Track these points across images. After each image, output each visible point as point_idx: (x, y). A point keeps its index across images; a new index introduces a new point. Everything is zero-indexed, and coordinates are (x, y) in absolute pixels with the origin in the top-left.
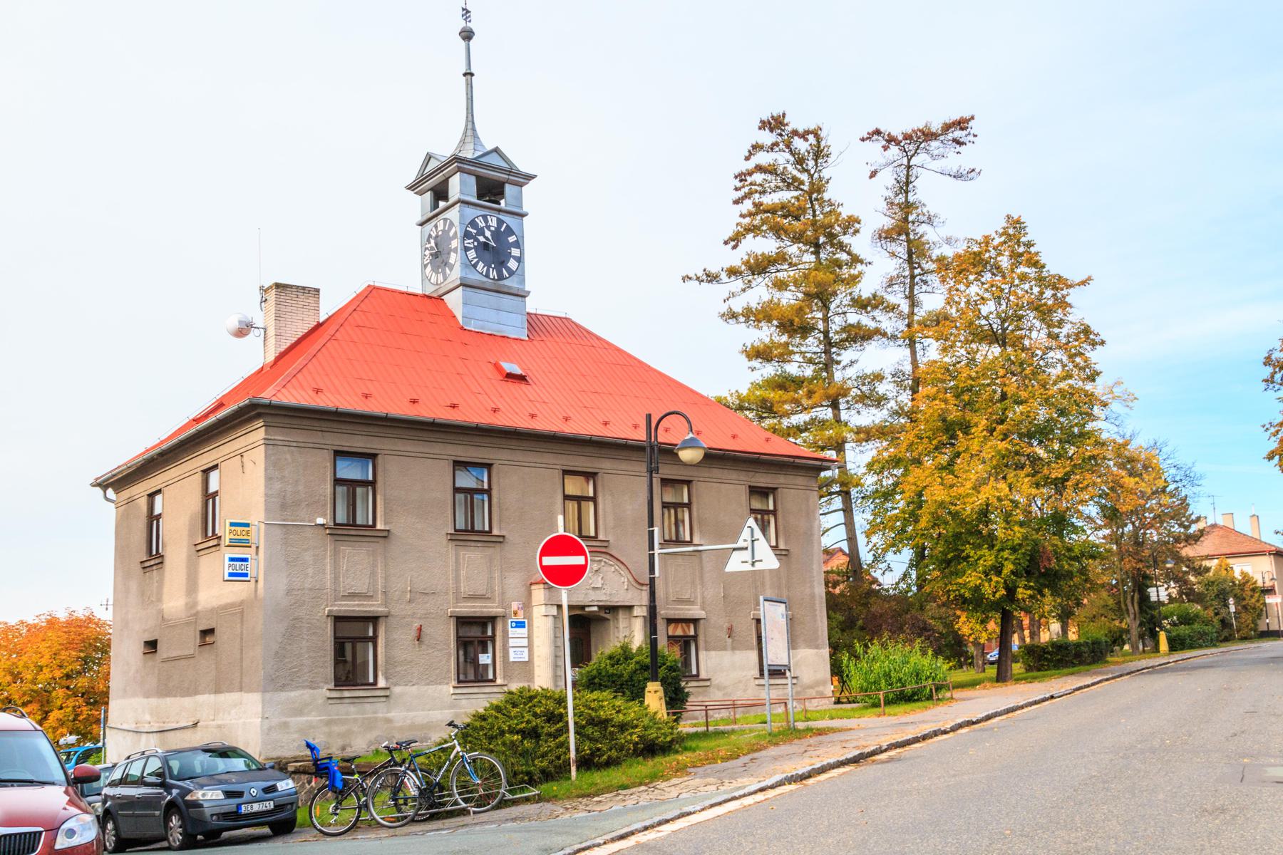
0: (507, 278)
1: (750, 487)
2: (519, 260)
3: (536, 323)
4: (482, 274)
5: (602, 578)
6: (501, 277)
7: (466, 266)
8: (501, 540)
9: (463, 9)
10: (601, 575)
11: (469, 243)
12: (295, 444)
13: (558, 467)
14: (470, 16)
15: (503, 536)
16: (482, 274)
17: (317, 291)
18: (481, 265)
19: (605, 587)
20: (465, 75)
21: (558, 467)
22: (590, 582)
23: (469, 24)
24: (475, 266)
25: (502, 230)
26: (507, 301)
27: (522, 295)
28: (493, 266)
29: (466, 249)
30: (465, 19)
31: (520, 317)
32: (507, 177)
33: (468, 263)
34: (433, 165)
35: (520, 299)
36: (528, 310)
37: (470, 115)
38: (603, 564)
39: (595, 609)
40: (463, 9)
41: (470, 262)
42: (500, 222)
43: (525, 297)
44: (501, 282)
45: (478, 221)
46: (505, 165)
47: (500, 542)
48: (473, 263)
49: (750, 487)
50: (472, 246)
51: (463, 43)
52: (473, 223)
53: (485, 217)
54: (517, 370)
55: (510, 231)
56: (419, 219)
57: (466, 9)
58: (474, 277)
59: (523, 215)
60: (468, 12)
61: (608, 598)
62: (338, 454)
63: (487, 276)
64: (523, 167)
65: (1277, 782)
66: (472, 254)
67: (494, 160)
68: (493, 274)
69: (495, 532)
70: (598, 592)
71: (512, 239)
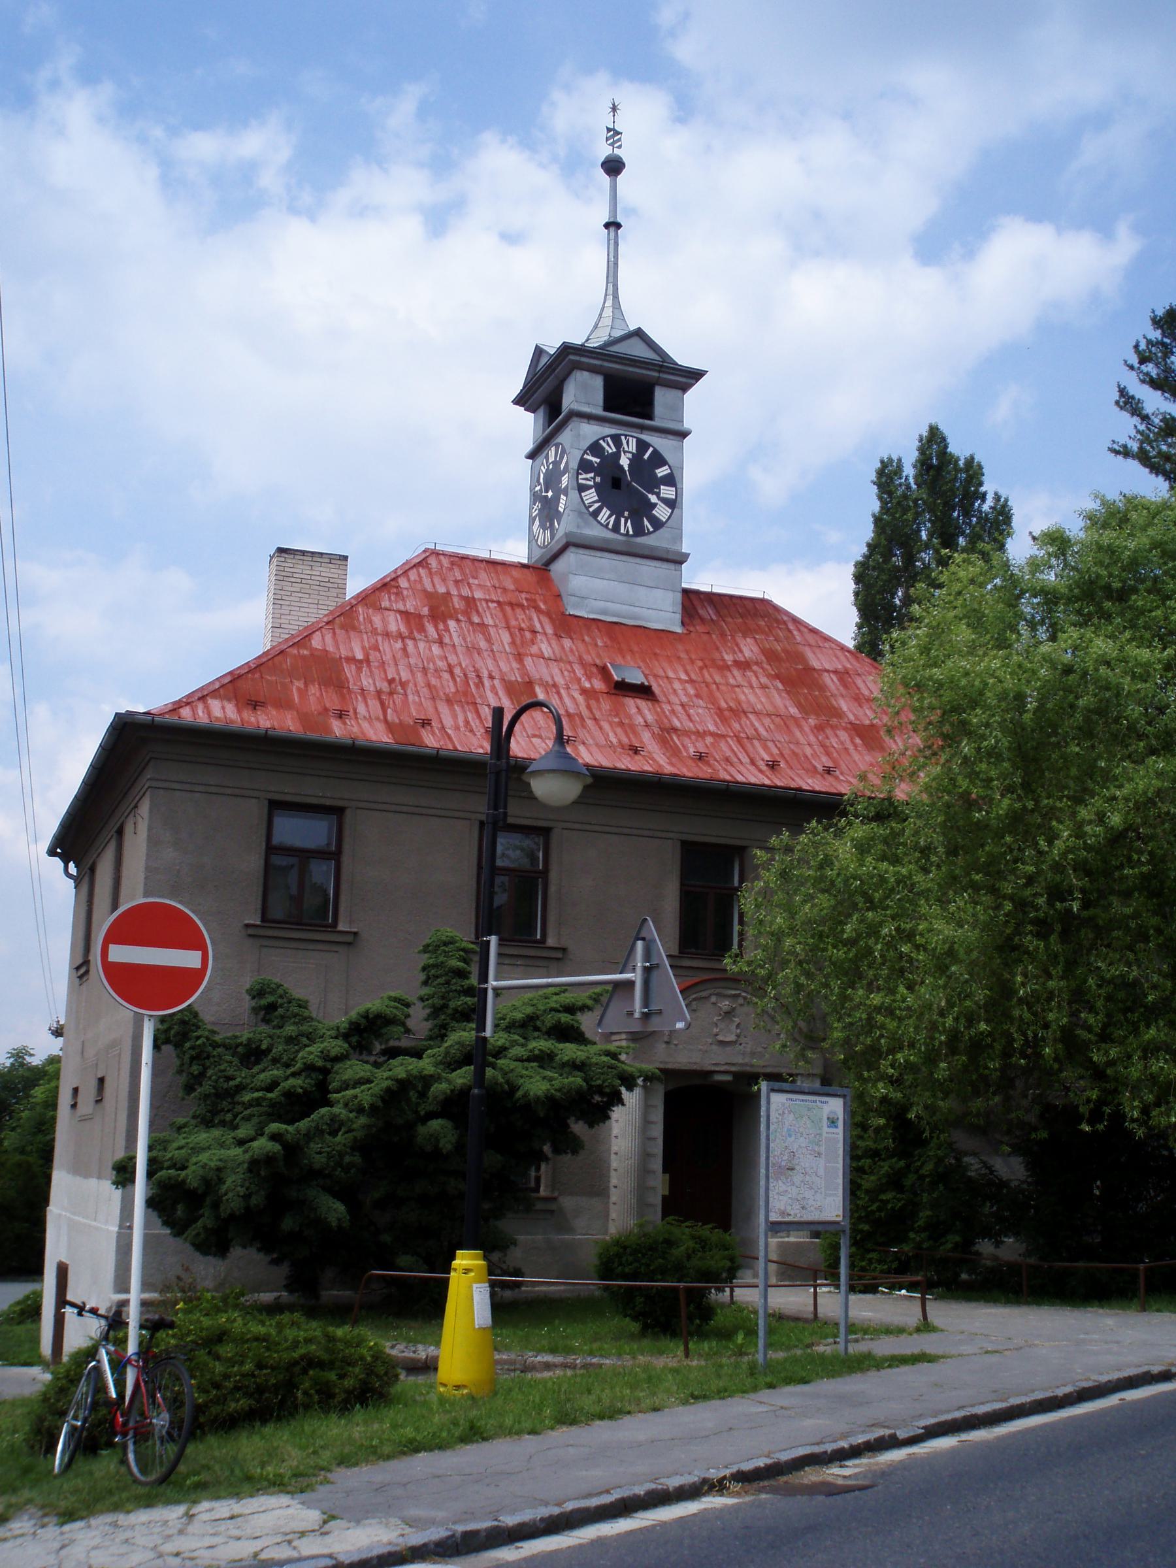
0: (649, 533)
1: (684, 843)
2: (672, 504)
3: (693, 601)
4: (606, 526)
5: (738, 1026)
6: (639, 531)
7: (580, 514)
8: (560, 955)
9: (609, 130)
10: (737, 1020)
11: (586, 478)
12: (201, 788)
13: (671, 835)
14: (619, 140)
15: (564, 950)
16: (606, 526)
17: (345, 558)
18: (605, 513)
19: (742, 1040)
20: (607, 226)
21: (671, 835)
22: (715, 1030)
23: (617, 151)
24: (596, 514)
25: (646, 457)
26: (649, 569)
27: (679, 560)
28: (626, 514)
29: (582, 488)
30: (612, 145)
31: (670, 594)
32: (656, 374)
33: (584, 510)
34: (544, 360)
35: (672, 566)
36: (684, 585)
37: (611, 286)
38: (741, 1001)
39: (729, 1078)
40: (609, 130)
41: (587, 508)
42: (642, 446)
43: (681, 563)
44: (639, 540)
45: (604, 445)
46: (648, 354)
47: (558, 959)
48: (591, 509)
49: (684, 843)
50: (591, 483)
51: (606, 179)
52: (595, 448)
53: (616, 439)
54: (635, 677)
55: (659, 460)
56: (529, 446)
57: (614, 130)
58: (594, 531)
59: (683, 434)
60: (617, 133)
61: (747, 1060)
62: (276, 806)
63: (616, 529)
64: (683, 358)
65: (260, 1537)
66: (591, 496)
67: (637, 350)
68: (627, 526)
69: (551, 942)
70: (728, 1049)
71: (662, 472)
